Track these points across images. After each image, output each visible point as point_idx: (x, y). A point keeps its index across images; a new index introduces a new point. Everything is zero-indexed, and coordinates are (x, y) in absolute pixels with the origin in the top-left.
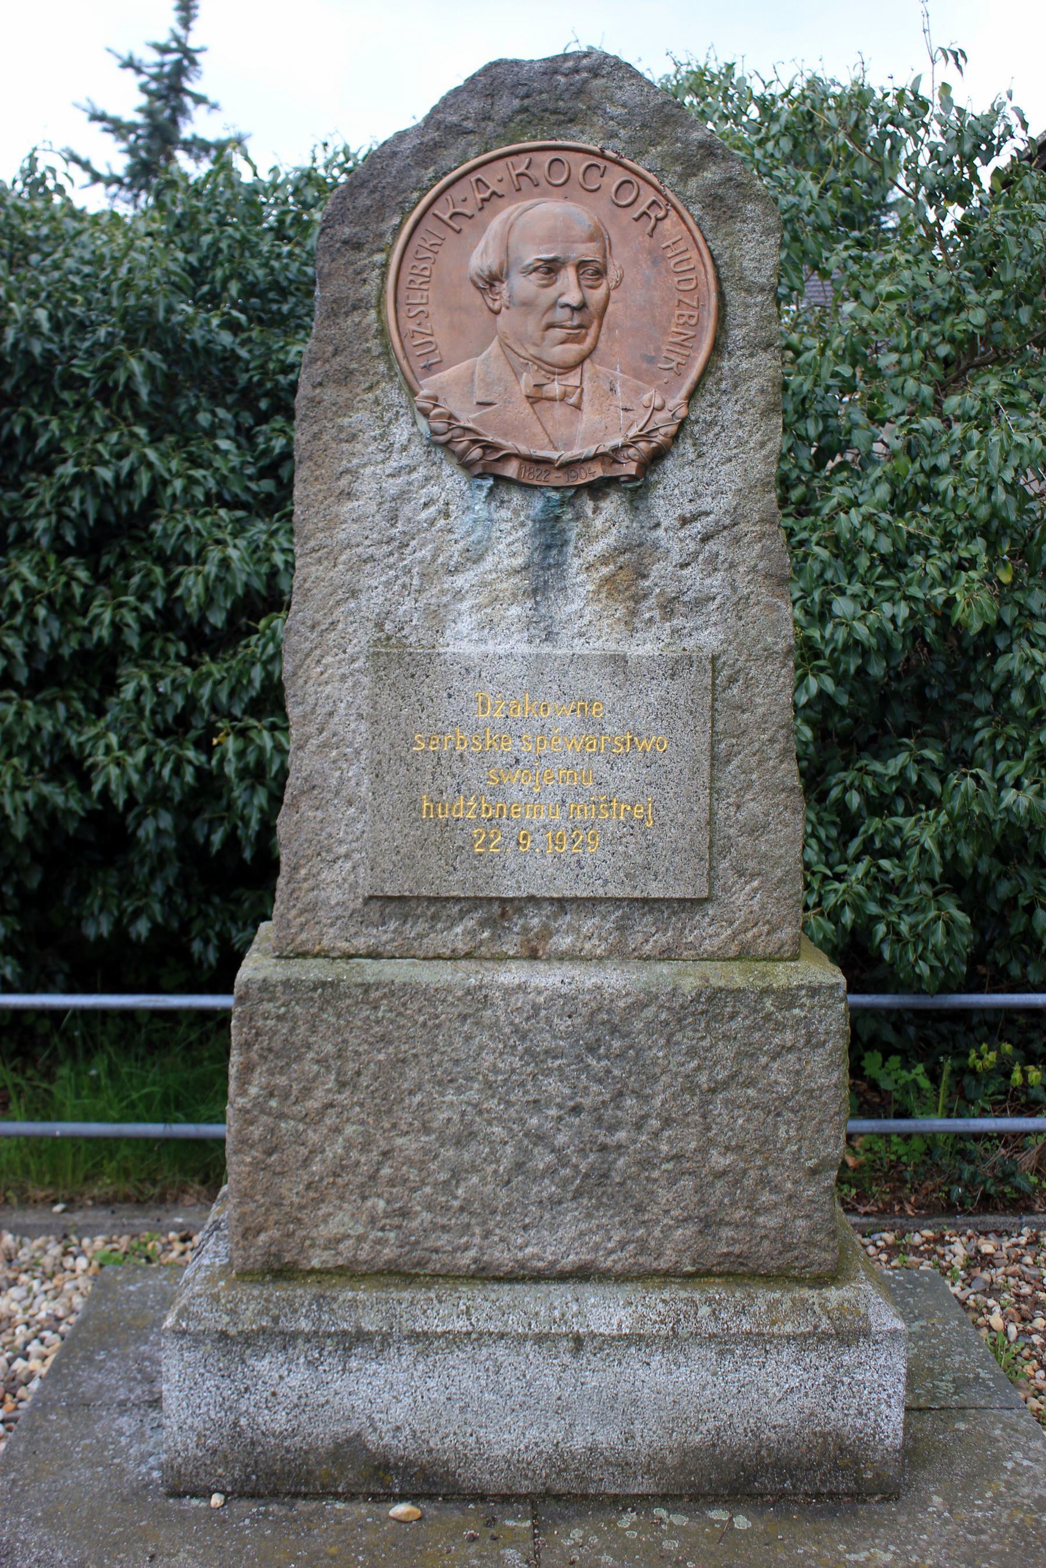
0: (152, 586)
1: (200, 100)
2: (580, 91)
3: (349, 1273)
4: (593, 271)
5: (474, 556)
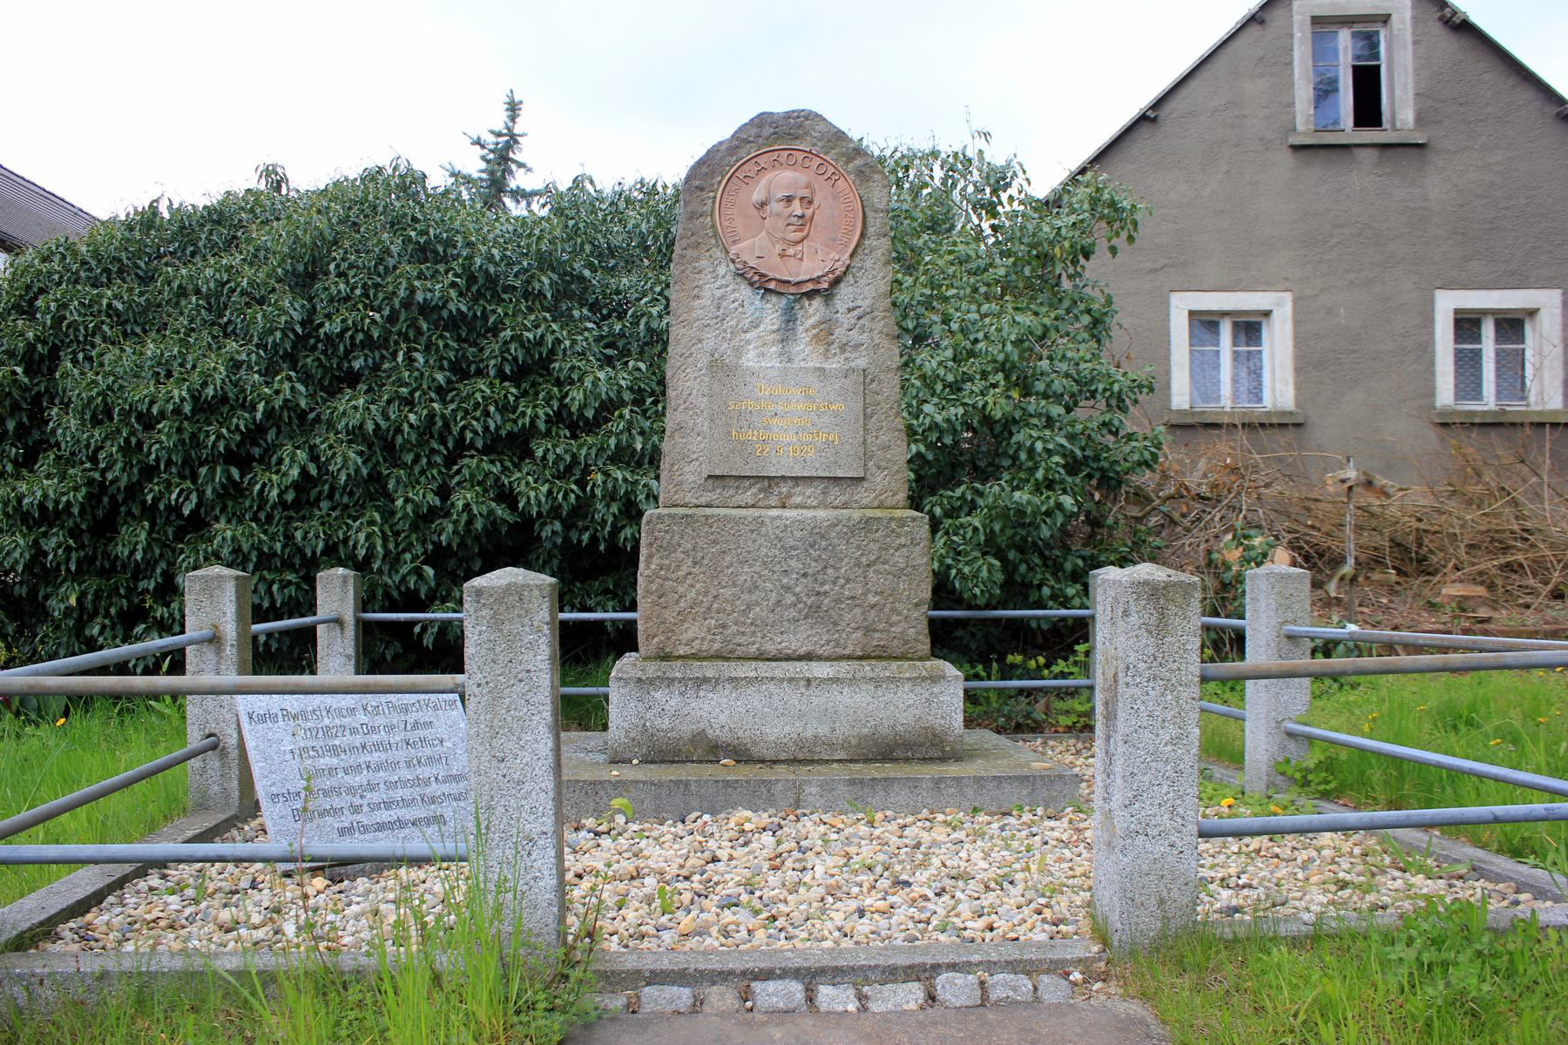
0: (551, 398)
1: (521, 165)
2: (800, 126)
3: (695, 657)
4: (807, 201)
5: (755, 325)
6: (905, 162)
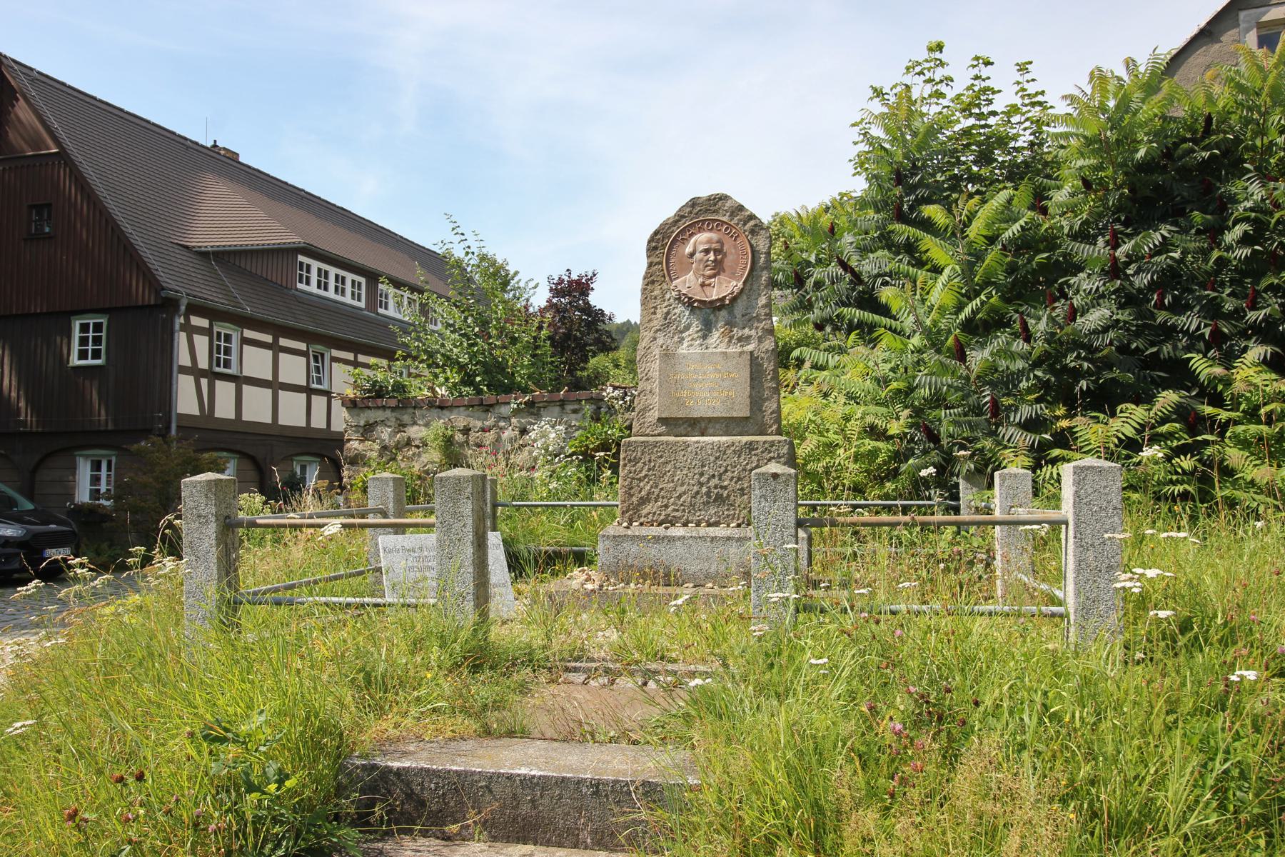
5: (687, 328)
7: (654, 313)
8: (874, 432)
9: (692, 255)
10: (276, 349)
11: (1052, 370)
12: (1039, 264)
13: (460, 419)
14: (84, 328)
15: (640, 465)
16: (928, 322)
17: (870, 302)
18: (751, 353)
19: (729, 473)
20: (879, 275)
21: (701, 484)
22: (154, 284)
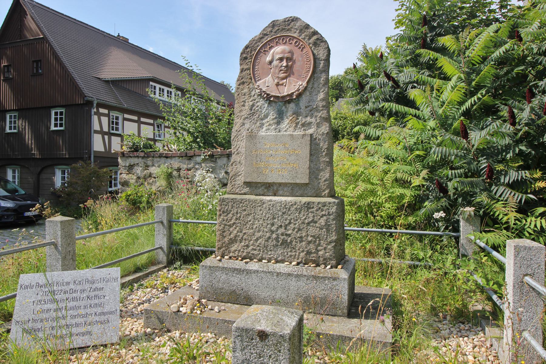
5: (266, 116)
6: (471, 65)
7: (244, 106)
8: (404, 183)
9: (271, 62)
10: (139, 123)
11: (530, 145)
12: (517, 74)
13: (176, 163)
14: (56, 114)
15: (230, 215)
16: (440, 111)
17: (403, 99)
18: (311, 135)
19: (292, 225)
20: (411, 83)
21: (272, 232)
22: (82, 94)
